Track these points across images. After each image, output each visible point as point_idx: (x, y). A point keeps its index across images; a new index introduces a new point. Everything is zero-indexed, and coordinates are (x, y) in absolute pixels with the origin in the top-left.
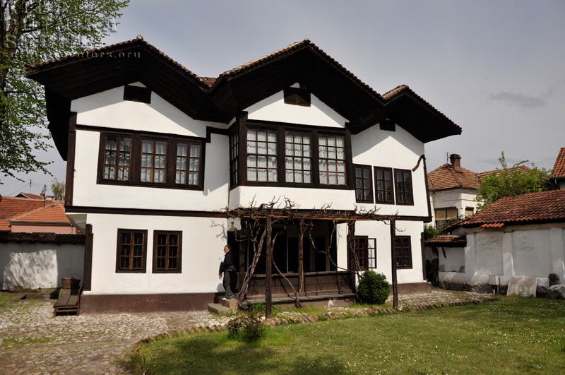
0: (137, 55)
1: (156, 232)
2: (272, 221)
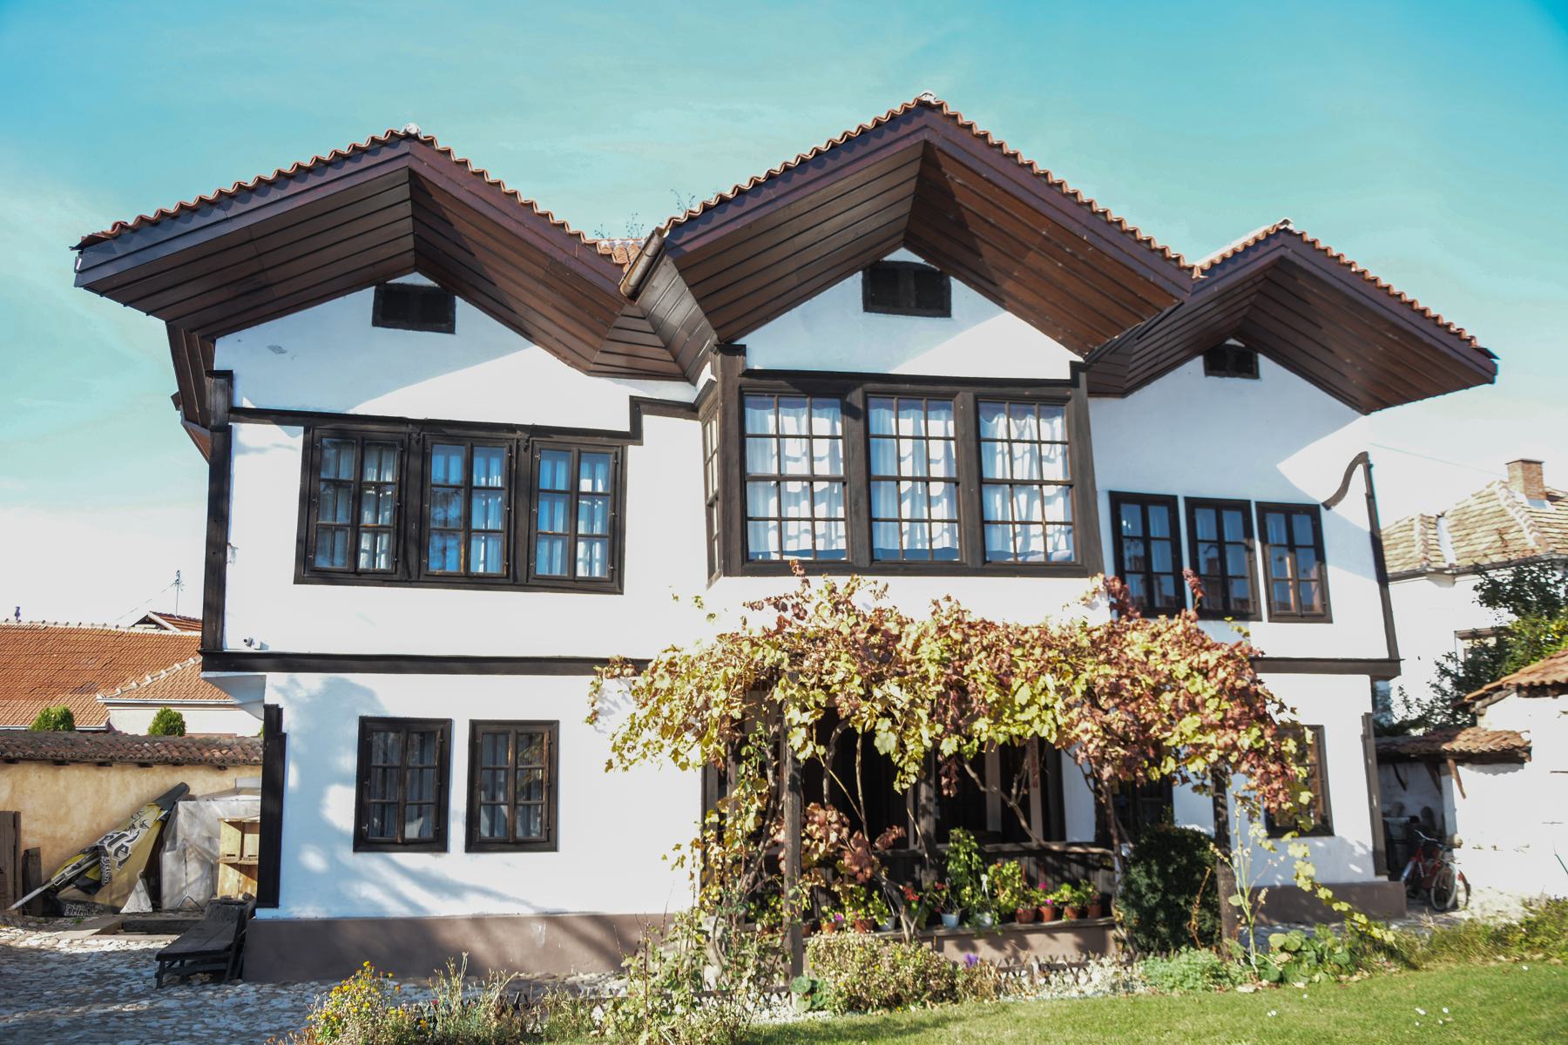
1: (475, 725)
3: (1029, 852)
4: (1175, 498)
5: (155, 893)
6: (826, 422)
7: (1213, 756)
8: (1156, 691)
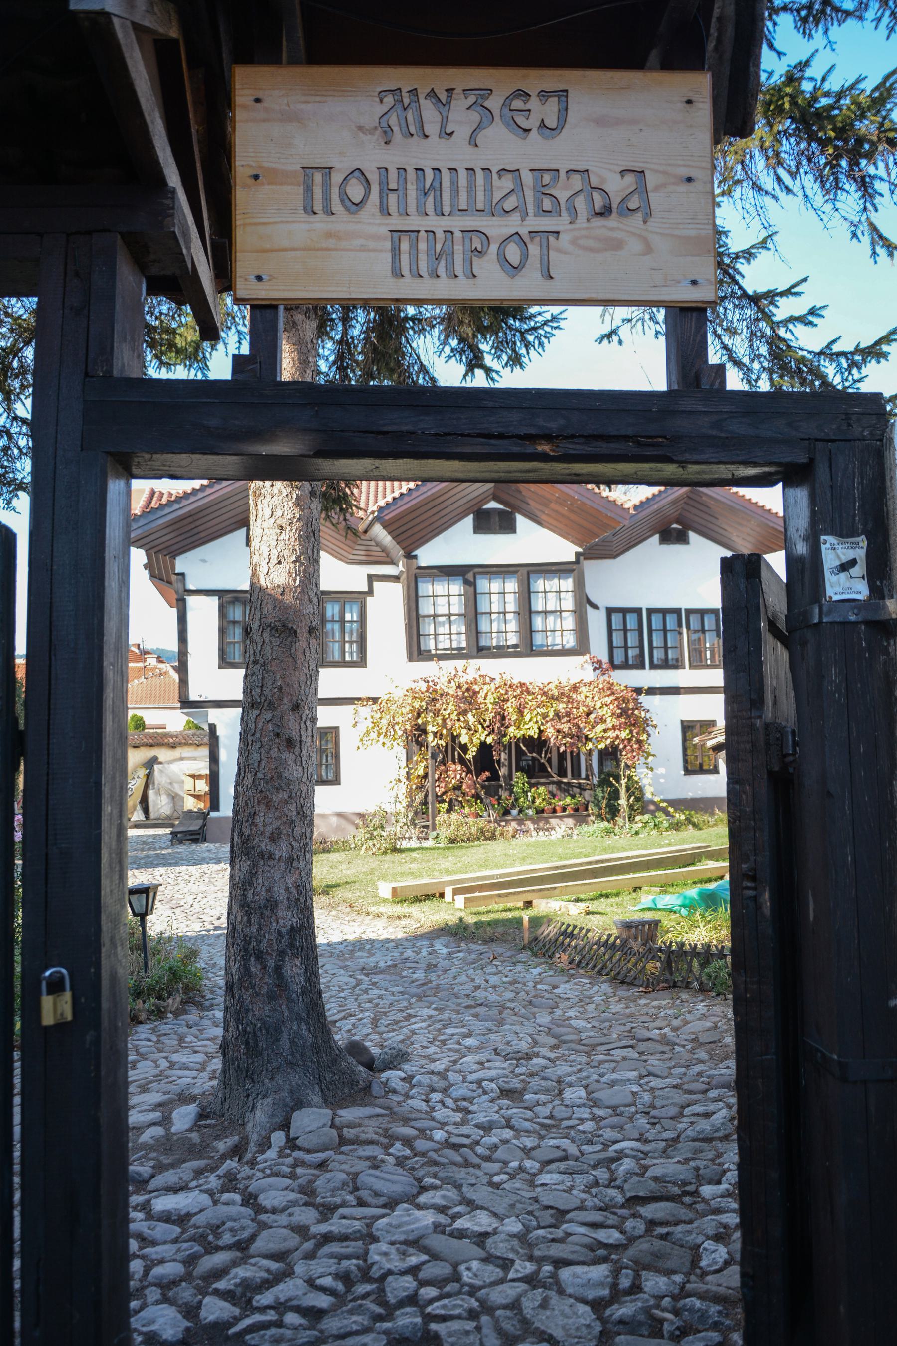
0: (305, 359)
2: (626, 765)
3: (553, 783)
4: (641, 609)
5: (146, 811)
6: (457, 587)
7: (608, 742)
8: (588, 714)
